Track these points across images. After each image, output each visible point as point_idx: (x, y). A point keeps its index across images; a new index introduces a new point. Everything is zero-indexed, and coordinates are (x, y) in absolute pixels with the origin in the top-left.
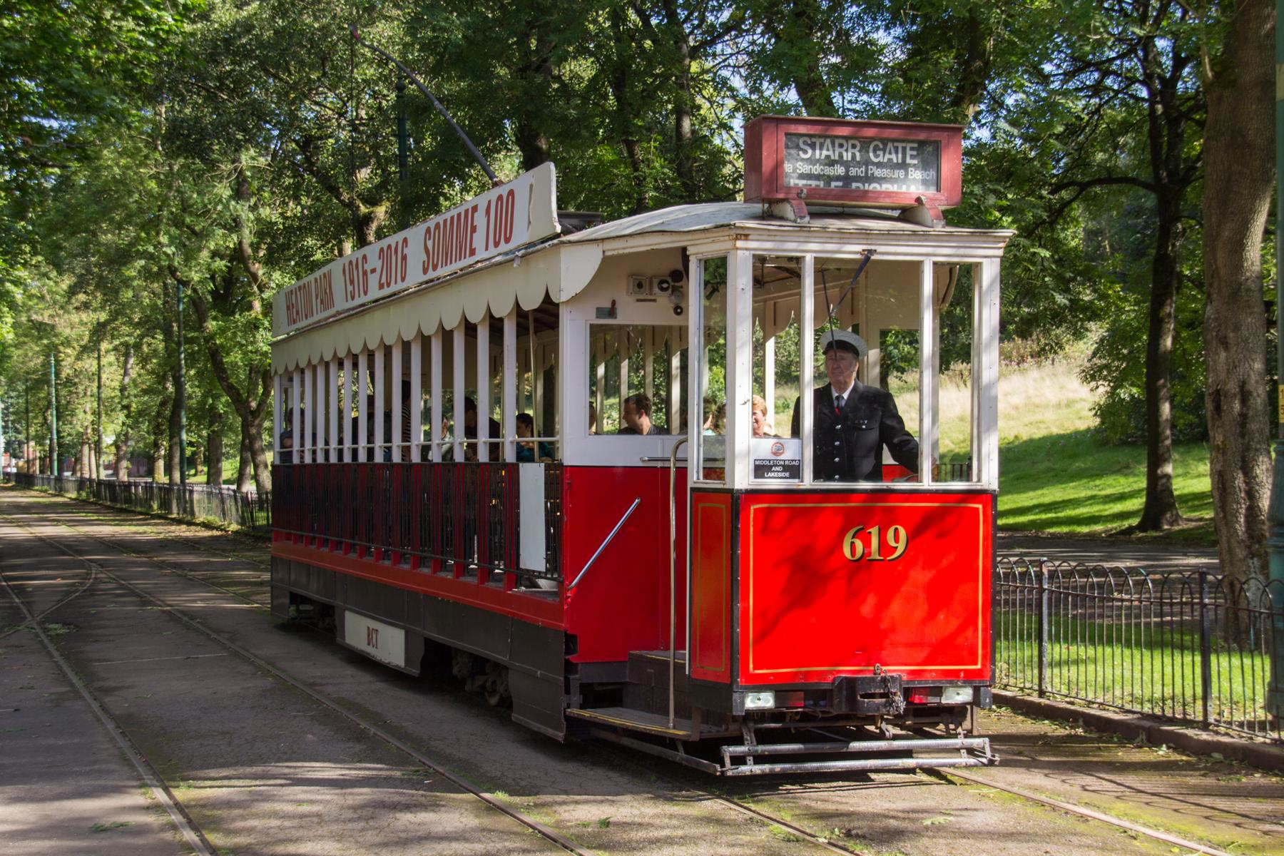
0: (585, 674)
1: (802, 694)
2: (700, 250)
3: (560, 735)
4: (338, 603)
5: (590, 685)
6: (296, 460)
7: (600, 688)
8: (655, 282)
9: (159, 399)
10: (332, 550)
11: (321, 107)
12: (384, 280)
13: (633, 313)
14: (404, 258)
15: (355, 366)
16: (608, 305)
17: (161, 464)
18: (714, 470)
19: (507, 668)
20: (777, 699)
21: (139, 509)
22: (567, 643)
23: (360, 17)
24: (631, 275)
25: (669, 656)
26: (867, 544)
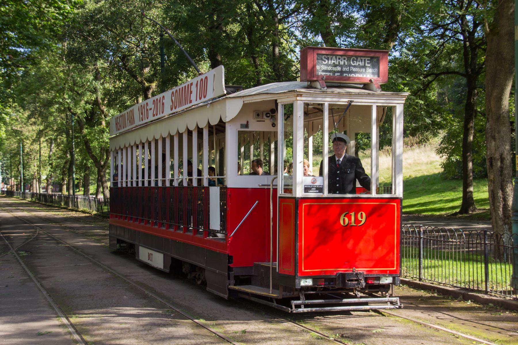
0: (236, 271)
1: (324, 280)
2: (282, 101)
3: (226, 296)
4: (136, 243)
5: (238, 276)
6: (119, 185)
7: (242, 277)
8: (264, 114)
9: (64, 161)
10: (134, 222)
11: (129, 43)
12: (155, 113)
13: (255, 126)
14: (163, 104)
15: (143, 147)
16: (245, 123)
17: (65, 187)
18: (288, 189)
19: (204, 269)
20: (313, 282)
21: (56, 205)
22: (229, 259)
23: (145, 7)
24: (255, 111)
25: (270, 264)
26: (350, 219)
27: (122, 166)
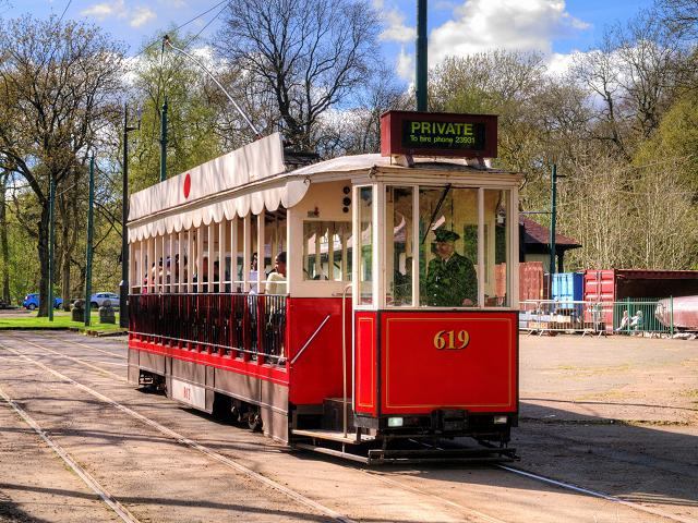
15: (186, 237)
16: (313, 210)
23: (252, 81)
27: (217, 264)
